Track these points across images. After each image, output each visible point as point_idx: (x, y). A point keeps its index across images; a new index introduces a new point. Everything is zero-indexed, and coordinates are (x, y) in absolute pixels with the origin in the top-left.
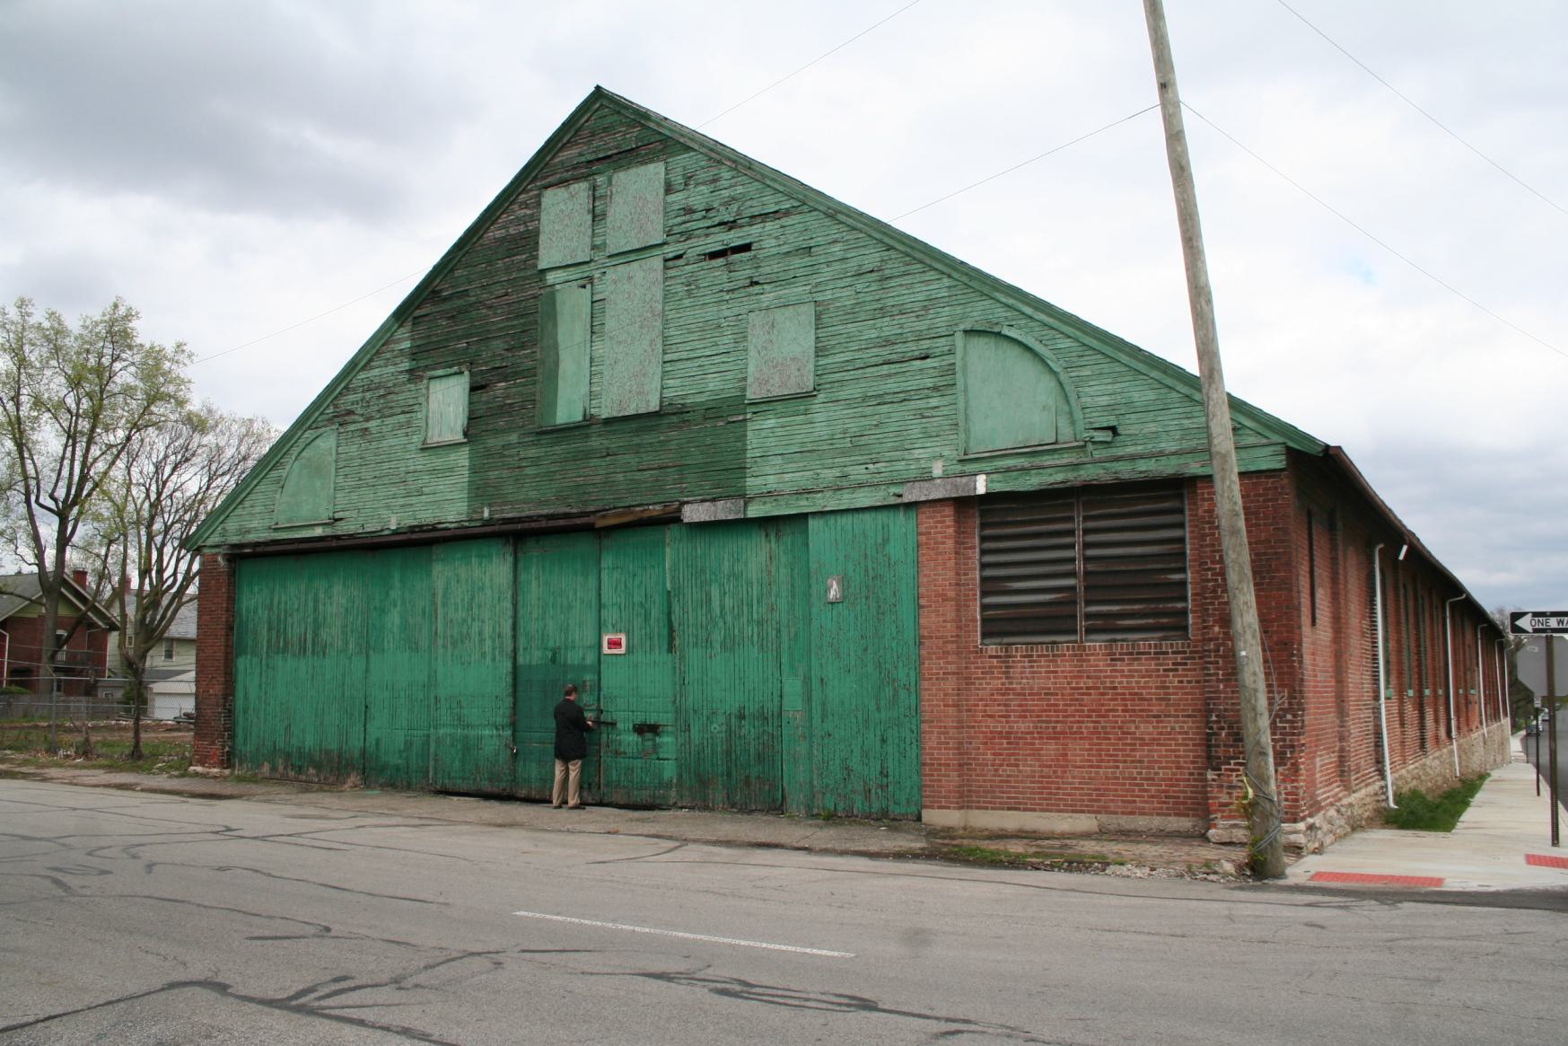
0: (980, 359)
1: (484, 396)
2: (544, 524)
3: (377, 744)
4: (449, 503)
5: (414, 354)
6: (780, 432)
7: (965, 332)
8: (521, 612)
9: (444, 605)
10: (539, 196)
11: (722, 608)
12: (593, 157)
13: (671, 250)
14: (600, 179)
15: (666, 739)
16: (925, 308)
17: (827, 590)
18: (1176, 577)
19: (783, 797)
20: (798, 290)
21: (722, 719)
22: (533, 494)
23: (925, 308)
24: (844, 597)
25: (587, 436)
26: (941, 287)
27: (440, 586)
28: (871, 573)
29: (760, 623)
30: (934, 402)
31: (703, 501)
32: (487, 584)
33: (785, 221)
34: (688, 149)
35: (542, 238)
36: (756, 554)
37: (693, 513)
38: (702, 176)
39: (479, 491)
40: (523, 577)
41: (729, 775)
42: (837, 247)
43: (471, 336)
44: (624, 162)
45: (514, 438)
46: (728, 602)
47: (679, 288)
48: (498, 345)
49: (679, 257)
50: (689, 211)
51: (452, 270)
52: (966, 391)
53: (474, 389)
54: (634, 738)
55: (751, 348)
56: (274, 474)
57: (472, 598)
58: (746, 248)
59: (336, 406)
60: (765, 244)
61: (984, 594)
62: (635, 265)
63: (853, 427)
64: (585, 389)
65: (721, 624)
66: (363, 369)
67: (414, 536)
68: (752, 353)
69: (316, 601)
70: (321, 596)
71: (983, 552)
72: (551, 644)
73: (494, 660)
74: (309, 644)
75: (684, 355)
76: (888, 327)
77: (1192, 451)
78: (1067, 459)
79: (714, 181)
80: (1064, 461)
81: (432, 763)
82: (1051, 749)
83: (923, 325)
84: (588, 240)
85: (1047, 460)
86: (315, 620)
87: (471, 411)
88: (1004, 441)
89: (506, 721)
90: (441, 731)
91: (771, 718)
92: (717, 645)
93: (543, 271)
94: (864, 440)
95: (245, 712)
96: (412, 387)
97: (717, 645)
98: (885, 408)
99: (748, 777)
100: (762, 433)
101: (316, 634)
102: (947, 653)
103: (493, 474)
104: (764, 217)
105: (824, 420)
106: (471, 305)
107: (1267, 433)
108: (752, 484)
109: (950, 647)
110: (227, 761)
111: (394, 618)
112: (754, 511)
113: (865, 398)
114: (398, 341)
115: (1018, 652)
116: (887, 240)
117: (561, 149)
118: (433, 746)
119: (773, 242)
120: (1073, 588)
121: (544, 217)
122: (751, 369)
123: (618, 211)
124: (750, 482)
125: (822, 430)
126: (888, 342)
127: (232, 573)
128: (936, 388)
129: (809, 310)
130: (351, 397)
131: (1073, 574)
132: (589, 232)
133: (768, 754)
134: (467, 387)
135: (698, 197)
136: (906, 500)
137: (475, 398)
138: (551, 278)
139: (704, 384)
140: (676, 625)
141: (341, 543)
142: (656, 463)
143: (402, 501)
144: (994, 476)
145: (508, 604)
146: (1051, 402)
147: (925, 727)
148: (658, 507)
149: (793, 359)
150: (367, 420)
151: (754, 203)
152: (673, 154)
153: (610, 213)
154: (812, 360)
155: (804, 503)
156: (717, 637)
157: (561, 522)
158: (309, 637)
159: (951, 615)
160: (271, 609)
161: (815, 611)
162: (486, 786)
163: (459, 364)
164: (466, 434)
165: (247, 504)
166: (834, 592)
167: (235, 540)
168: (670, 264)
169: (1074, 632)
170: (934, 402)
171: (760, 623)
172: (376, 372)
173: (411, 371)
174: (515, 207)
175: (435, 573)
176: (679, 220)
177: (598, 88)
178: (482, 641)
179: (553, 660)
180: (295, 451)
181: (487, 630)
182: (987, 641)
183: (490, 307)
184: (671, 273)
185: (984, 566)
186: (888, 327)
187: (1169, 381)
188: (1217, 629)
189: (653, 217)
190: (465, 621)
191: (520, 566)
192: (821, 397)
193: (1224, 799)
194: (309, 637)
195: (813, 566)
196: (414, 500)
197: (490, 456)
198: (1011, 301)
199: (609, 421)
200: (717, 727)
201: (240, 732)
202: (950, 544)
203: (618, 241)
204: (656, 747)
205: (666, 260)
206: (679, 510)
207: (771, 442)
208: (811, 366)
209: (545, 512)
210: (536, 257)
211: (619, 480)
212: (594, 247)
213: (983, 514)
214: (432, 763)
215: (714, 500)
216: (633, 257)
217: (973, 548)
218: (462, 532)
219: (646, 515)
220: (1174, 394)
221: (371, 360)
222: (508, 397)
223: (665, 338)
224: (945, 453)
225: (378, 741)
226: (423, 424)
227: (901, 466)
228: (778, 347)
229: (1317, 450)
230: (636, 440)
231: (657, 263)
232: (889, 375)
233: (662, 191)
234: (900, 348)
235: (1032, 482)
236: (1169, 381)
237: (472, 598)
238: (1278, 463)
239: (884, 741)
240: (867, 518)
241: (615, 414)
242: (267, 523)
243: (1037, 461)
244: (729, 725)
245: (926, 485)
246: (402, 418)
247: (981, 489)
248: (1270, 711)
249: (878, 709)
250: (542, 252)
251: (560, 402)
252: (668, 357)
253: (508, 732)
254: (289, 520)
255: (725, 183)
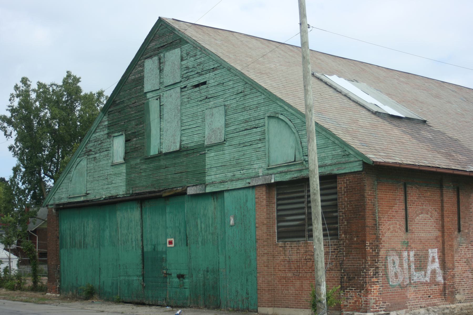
0: (274, 128)
1: (130, 144)
2: (148, 195)
3: (103, 284)
4: (119, 188)
5: (109, 127)
6: (216, 158)
7: (268, 117)
8: (144, 230)
9: (121, 228)
10: (144, 62)
11: (201, 228)
12: (159, 46)
13: (183, 85)
14: (162, 55)
15: (186, 280)
16: (257, 107)
17: (230, 221)
18: (335, 214)
19: (220, 303)
20: (220, 101)
21: (202, 272)
22: (145, 183)
23: (257, 107)
24: (235, 223)
25: (160, 160)
26: (261, 99)
27: (119, 220)
28: (243, 214)
29: (213, 234)
30: (260, 145)
31: (193, 186)
32: (133, 219)
33: (216, 72)
34: (187, 43)
35: (145, 79)
36: (210, 206)
37: (191, 191)
38: (192, 53)
39: (129, 182)
40: (144, 216)
41: (204, 294)
42: (231, 83)
43: (125, 119)
44: (169, 48)
45: (138, 161)
46: (203, 226)
47: (186, 100)
48: (133, 123)
49: (185, 87)
50: (187, 68)
51: (119, 93)
52: (268, 141)
53: (127, 141)
54: (177, 280)
55: (206, 124)
56: (68, 175)
57: (129, 225)
58: (204, 83)
59: (86, 148)
60: (210, 82)
61: (278, 222)
62: (172, 90)
63: (236, 155)
64: (158, 141)
65: (201, 234)
66: (94, 133)
67: (111, 200)
68: (207, 126)
69: (84, 227)
70: (85, 224)
71: (278, 205)
72: (153, 243)
73: (136, 249)
74: (82, 244)
75: (187, 127)
76: (246, 115)
77: (335, 164)
78: (298, 167)
79: (195, 56)
80: (297, 169)
81: (119, 291)
82: (298, 283)
83: (256, 115)
84: (158, 80)
85: (293, 168)
86: (84, 234)
87: (126, 150)
88: (280, 162)
89: (140, 274)
90: (122, 278)
91: (216, 271)
92: (200, 243)
93: (146, 93)
94: (240, 161)
95: (64, 272)
96: (108, 140)
97: (200, 243)
98: (245, 148)
99: (210, 295)
100: (211, 158)
101: (84, 240)
102: (264, 245)
103: (133, 175)
104: (209, 71)
105: (229, 153)
106: (125, 107)
107: (357, 156)
108: (208, 179)
109: (265, 243)
110: (59, 291)
111: (107, 233)
112: (208, 190)
113: (240, 144)
114: (104, 122)
115: (288, 245)
116: (245, 80)
117: (150, 43)
118: (119, 283)
119: (213, 81)
120: (303, 219)
121: (145, 71)
122: (206, 133)
123: (167, 68)
124: (207, 178)
125: (227, 157)
126: (246, 121)
127: (58, 216)
128: (260, 140)
129: (222, 108)
130: (91, 145)
131: (304, 214)
132: (159, 77)
133: (215, 287)
134: (124, 140)
135: (190, 62)
136: (251, 185)
137: (127, 145)
138: (149, 95)
139: (191, 140)
140: (188, 235)
141: (89, 203)
142: (180, 171)
143: (106, 187)
144: (277, 175)
145: (139, 227)
146: (294, 145)
147: (258, 275)
148: (180, 188)
149: (218, 128)
150: (95, 154)
151: (207, 65)
152: (183, 45)
153: (165, 69)
154: (224, 129)
155: (222, 186)
156: (200, 240)
157: (153, 195)
158: (82, 241)
159: (265, 231)
160: (70, 230)
161: (226, 229)
162: (136, 300)
163: (122, 131)
164: (124, 159)
165: (61, 188)
166: (232, 222)
167: (57, 202)
168: (183, 90)
169: (304, 237)
170: (260, 145)
171: (213, 234)
172: (98, 134)
173: (108, 134)
174: (137, 66)
175: (117, 215)
176: (185, 72)
177: (159, 18)
178: (132, 242)
179: (154, 249)
180: (75, 166)
181: (134, 238)
182: (279, 241)
183: (130, 108)
184: (183, 93)
185: (278, 210)
186: (246, 115)
187: (328, 136)
188: (343, 235)
189: (177, 71)
190: (127, 234)
191: (143, 212)
192: (227, 144)
193: (346, 303)
194: (82, 241)
195: (226, 211)
196: (110, 186)
197: (131, 168)
198: (281, 104)
199: (166, 154)
200: (200, 275)
201: (62, 279)
202: (264, 203)
203: (168, 81)
204: (183, 283)
205: (182, 88)
206: (186, 190)
207: (213, 162)
208: (223, 132)
209: (148, 190)
210: (143, 87)
211: (169, 178)
212: (161, 83)
213: (278, 189)
214: (119, 291)
215: (196, 185)
216: (172, 87)
217: (274, 203)
218: (124, 199)
219: (177, 191)
220: (330, 141)
221: (96, 129)
222: (136, 144)
223: (182, 120)
224: (263, 166)
225: (103, 282)
226: (112, 155)
227: (250, 171)
228: (214, 125)
229: (371, 163)
230: (174, 162)
231: (178, 90)
232: (246, 135)
233: (180, 60)
234: (250, 124)
235: (287, 177)
236: (328, 136)
237: (129, 225)
238: (359, 169)
239: (247, 280)
240: (241, 192)
241: (167, 151)
242: (67, 195)
243: (289, 168)
244: (204, 274)
245: (257, 179)
246: (106, 153)
247: (273, 181)
248: (325, 268)
249: (245, 268)
250: (145, 85)
251: (152, 147)
252: (183, 128)
253: (141, 278)
254: (73, 194)
255: (198, 57)
